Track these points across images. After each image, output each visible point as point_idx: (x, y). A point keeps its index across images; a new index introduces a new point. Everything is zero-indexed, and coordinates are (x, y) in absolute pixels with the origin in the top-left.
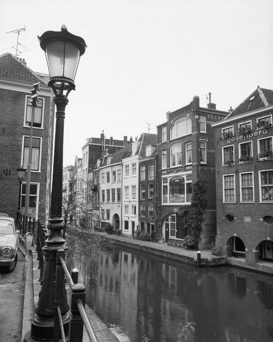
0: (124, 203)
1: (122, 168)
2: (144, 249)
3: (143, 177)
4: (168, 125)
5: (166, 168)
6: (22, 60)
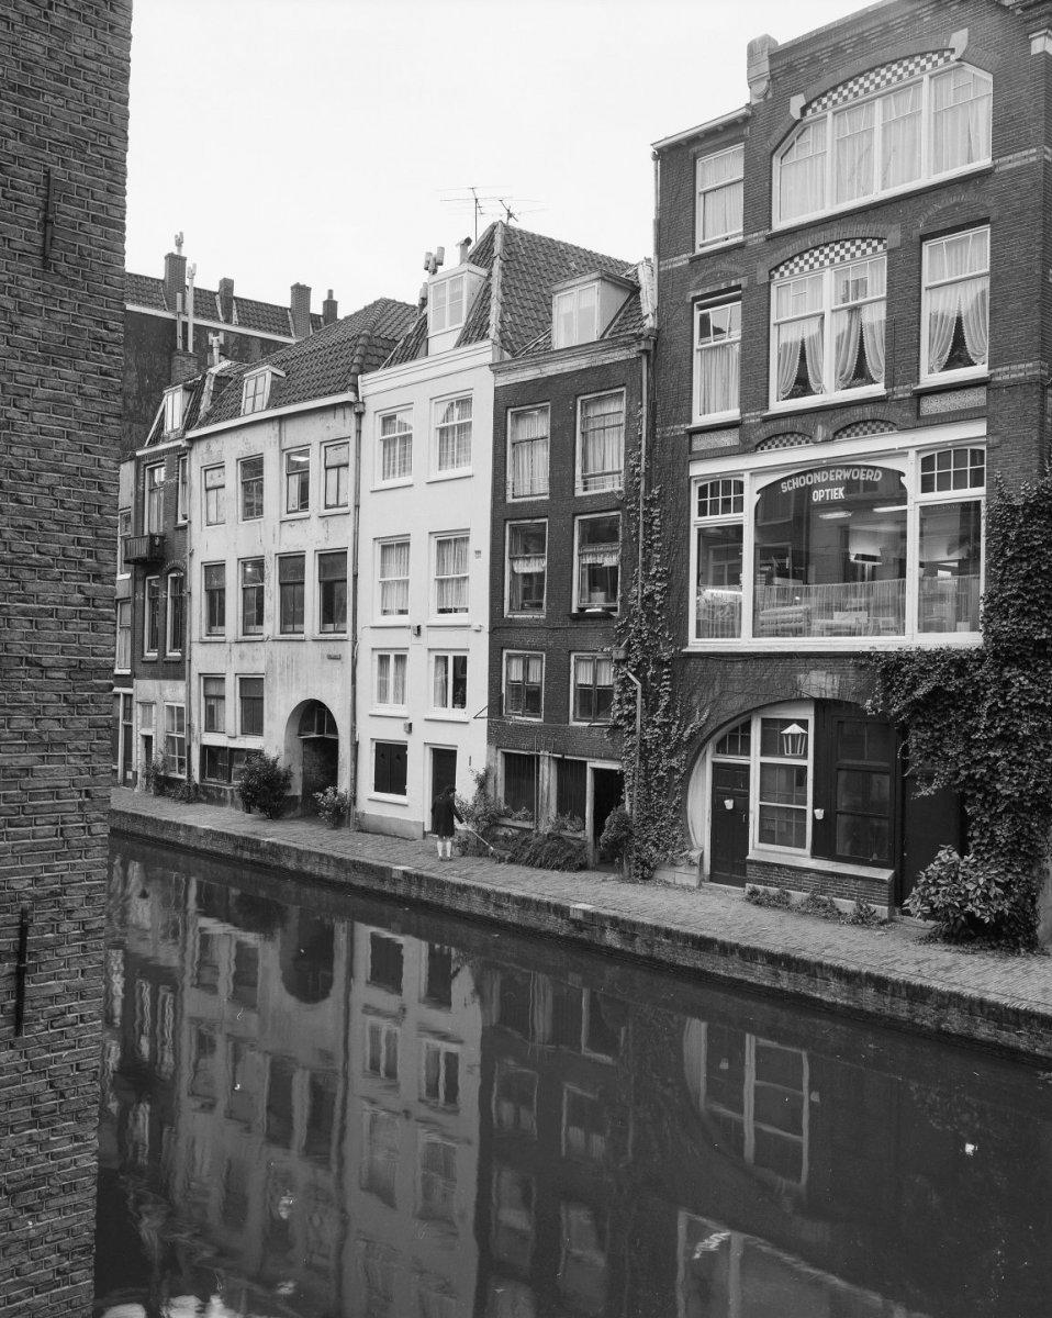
0: (368, 640)
1: (359, 432)
2: (611, 938)
3: (532, 478)
4: (760, 134)
5: (738, 411)
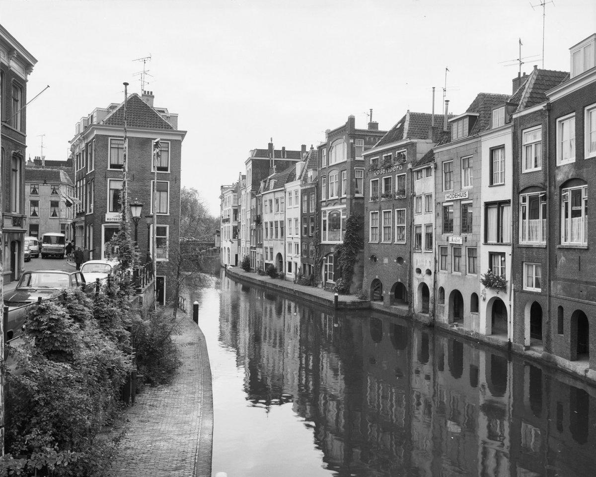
0: (287, 240)
3: (305, 211)
6: (150, 94)
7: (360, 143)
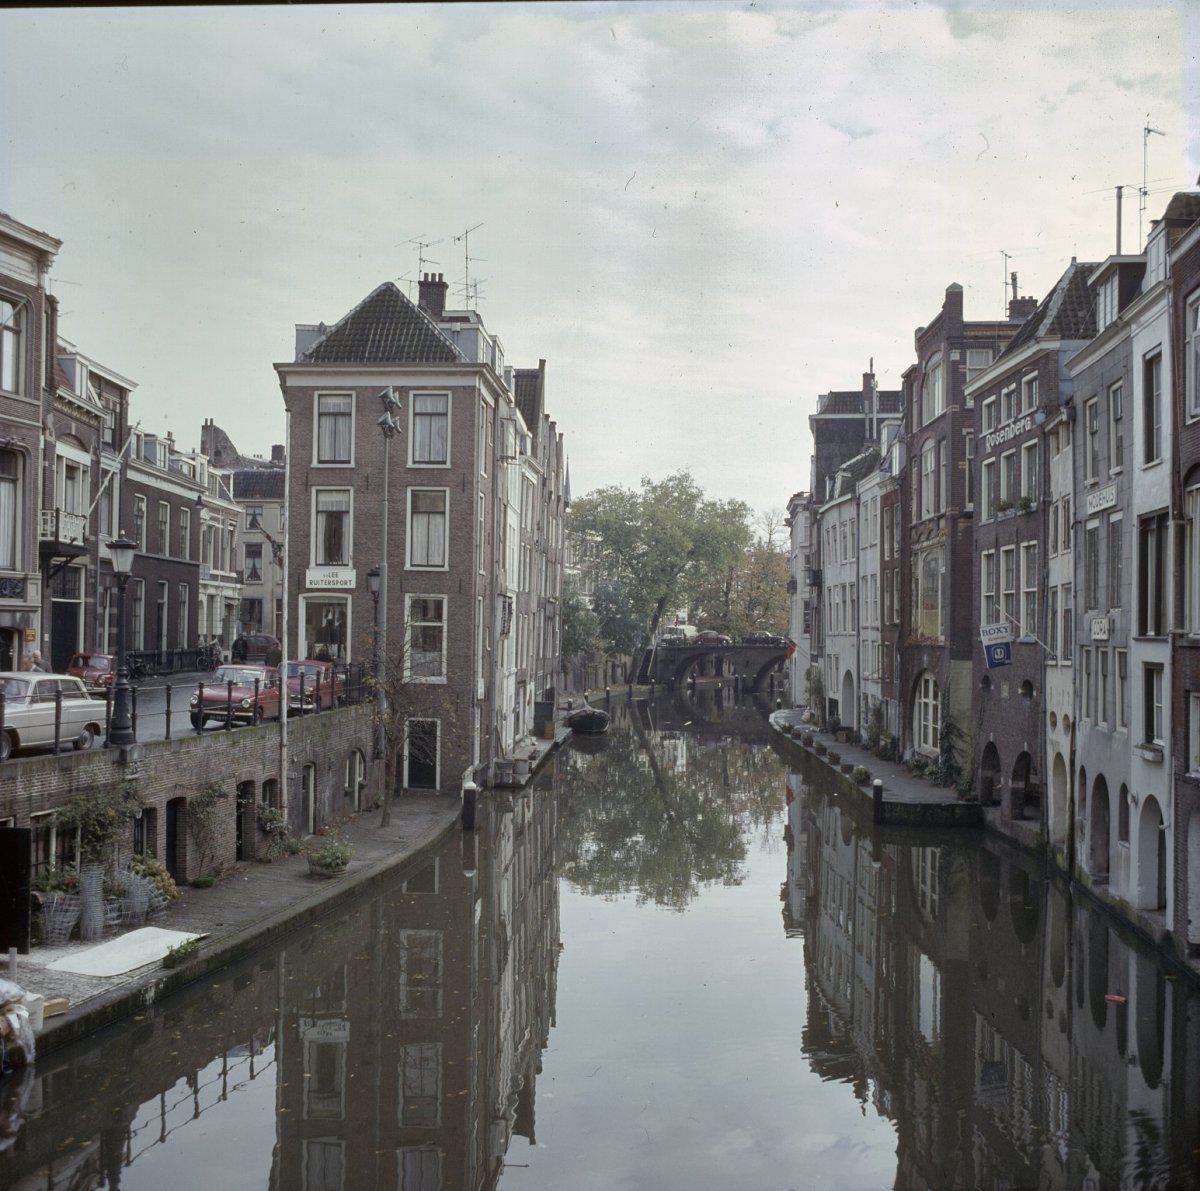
7: (975, 360)
